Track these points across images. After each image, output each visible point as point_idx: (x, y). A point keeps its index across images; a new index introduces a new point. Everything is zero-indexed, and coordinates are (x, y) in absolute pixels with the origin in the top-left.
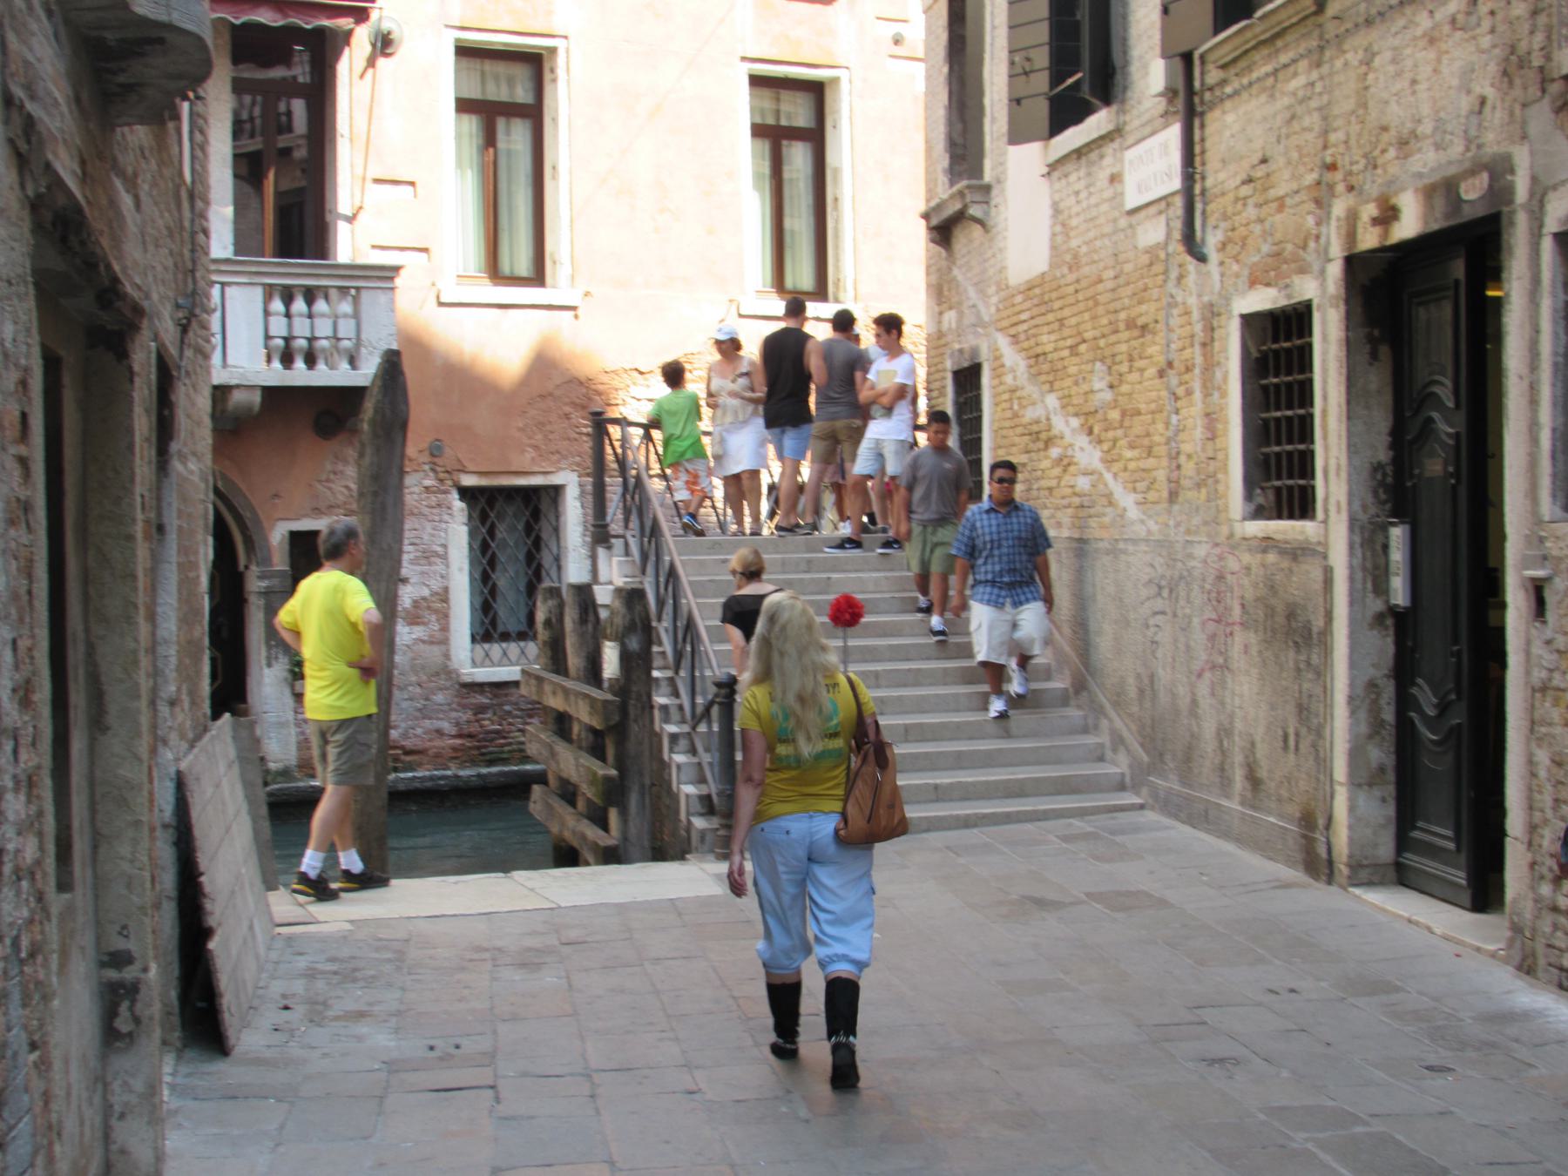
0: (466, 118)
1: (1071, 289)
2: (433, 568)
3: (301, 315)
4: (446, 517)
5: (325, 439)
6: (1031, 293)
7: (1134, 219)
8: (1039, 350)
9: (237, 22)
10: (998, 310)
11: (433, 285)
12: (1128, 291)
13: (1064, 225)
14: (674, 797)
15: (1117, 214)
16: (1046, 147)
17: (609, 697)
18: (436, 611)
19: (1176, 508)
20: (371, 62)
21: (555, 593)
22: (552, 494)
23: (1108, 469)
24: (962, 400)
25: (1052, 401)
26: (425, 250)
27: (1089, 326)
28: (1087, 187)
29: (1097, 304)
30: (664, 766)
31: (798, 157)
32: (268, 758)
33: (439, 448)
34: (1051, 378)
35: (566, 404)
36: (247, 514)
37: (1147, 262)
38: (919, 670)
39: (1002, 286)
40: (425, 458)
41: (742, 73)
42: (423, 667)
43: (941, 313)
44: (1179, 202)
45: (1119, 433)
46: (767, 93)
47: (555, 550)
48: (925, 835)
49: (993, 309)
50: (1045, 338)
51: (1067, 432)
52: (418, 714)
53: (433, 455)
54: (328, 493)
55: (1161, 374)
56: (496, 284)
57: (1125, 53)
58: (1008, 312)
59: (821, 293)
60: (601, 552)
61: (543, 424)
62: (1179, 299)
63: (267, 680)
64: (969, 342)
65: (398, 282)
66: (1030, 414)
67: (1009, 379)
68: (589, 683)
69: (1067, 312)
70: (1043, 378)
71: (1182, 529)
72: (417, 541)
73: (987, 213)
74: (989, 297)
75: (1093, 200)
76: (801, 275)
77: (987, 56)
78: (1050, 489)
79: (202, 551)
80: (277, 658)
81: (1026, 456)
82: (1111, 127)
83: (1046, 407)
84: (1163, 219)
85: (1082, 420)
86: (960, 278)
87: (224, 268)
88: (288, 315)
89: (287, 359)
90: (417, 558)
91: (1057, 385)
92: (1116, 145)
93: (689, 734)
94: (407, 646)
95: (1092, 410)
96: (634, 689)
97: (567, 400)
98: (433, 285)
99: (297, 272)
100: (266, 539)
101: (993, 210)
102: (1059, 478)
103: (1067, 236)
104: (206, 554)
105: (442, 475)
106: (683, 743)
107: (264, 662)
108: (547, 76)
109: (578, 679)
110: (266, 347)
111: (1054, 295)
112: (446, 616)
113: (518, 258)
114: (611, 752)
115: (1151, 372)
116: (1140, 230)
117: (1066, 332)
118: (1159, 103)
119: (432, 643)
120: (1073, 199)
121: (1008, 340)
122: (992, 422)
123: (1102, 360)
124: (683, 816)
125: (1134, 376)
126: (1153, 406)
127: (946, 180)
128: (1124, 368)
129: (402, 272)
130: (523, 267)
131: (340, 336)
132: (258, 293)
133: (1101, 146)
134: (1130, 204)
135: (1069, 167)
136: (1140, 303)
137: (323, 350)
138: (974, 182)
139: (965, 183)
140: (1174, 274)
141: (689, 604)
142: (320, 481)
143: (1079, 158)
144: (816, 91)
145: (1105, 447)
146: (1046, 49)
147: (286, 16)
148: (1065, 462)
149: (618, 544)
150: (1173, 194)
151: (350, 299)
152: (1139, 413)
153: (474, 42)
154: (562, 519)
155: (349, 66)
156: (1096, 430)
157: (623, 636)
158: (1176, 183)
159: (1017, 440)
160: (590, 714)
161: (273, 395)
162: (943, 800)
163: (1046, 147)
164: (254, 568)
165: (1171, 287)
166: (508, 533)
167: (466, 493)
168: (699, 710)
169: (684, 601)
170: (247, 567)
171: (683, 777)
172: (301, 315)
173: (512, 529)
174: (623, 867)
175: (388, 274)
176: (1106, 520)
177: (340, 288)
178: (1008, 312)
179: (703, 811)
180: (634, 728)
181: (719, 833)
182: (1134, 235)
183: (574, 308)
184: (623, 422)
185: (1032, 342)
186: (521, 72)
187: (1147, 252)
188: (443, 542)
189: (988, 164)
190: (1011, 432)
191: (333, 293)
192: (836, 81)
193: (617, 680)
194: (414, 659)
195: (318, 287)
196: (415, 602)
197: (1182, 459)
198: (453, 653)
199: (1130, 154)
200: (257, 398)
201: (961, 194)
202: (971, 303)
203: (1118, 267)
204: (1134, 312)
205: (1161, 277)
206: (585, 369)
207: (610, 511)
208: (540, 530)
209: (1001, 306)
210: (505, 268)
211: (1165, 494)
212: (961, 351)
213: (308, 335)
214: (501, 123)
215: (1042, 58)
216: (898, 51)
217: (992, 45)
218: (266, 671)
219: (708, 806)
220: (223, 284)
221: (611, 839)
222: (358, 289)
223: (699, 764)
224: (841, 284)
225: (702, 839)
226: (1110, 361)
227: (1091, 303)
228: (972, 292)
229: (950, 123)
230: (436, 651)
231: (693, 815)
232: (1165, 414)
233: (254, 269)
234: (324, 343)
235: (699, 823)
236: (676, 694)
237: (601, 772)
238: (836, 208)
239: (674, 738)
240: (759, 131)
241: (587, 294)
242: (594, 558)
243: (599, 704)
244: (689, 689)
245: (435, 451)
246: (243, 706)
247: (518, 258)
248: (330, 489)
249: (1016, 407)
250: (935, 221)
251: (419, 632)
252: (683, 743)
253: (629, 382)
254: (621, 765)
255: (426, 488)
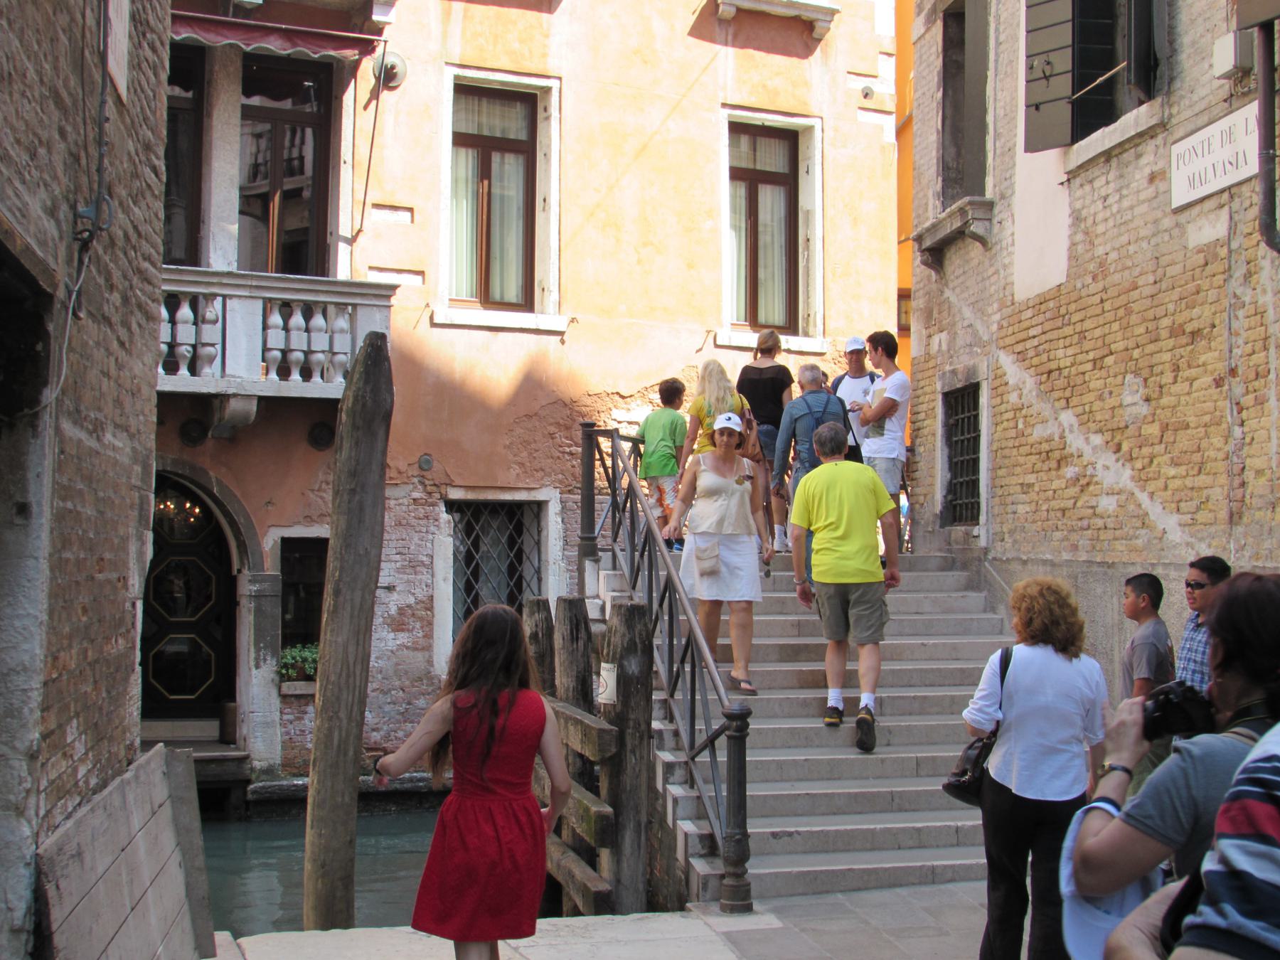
0: (462, 151)
1: (1097, 299)
2: (419, 577)
3: (299, 329)
4: (432, 529)
5: (320, 450)
6: (1043, 307)
7: (1182, 218)
8: (1053, 365)
9: (249, 49)
10: (1001, 328)
11: (428, 305)
12: (1175, 295)
13: (1087, 233)
14: (672, 834)
15: (1159, 214)
16: (1066, 154)
17: (606, 726)
18: (421, 619)
19: (1239, 530)
20: (375, 95)
21: (543, 605)
22: (535, 508)
23: (1143, 489)
24: (952, 421)
25: (1067, 417)
26: (421, 273)
27: (1119, 336)
28: (1119, 190)
29: (1129, 312)
30: (655, 796)
31: (771, 200)
32: (252, 756)
33: (428, 462)
34: (1068, 393)
35: (551, 424)
36: (241, 520)
37: (1202, 262)
38: (925, 697)
39: (1007, 302)
40: (415, 471)
41: (724, 116)
42: (406, 673)
43: (930, 336)
44: (1258, 186)
45: (1159, 449)
46: (745, 140)
47: (536, 564)
48: (950, 886)
49: (994, 327)
50: (1060, 353)
51: (1087, 450)
52: (400, 717)
53: (421, 468)
54: (320, 501)
55: (1218, 383)
56: (486, 308)
57: (1172, 42)
58: (1016, 328)
59: (791, 326)
60: (588, 565)
61: (529, 444)
62: (1247, 299)
63: (254, 681)
64: (963, 362)
65: (393, 300)
66: (1038, 433)
67: (1013, 398)
68: (578, 705)
69: (1088, 324)
70: (1056, 394)
71: (1247, 554)
72: (406, 551)
73: (989, 230)
74: (989, 316)
75: (1126, 203)
76: (772, 309)
77: (990, 74)
78: (1064, 511)
79: (133, 548)
80: (265, 660)
81: (1034, 476)
82: (1153, 121)
83: (1060, 424)
84: (1224, 213)
85: (1108, 436)
86: (953, 299)
87: (225, 281)
88: (286, 328)
89: (284, 372)
90: (404, 567)
91: (1074, 401)
92: (1159, 140)
93: (686, 763)
94: (392, 651)
95: (1122, 425)
96: (632, 716)
97: (552, 421)
98: (428, 305)
99: (297, 287)
100: (259, 544)
101: (996, 228)
102: (1076, 499)
103: (1092, 243)
104: (141, 554)
105: (429, 488)
106: (679, 773)
107: (252, 663)
108: (541, 115)
109: (566, 700)
110: (264, 360)
111: (1073, 307)
112: (430, 624)
113: (509, 284)
114: (604, 785)
115: (1207, 380)
116: (1191, 228)
117: (1087, 345)
118: (1221, 86)
119: (416, 649)
120: (1100, 205)
121: (1012, 357)
122: (991, 443)
123: (1136, 373)
124: (680, 854)
125: (1181, 387)
126: (1207, 418)
127: (938, 204)
128: (1168, 378)
129: (398, 291)
130: (513, 292)
131: (336, 350)
132: (259, 305)
133: (1137, 145)
134: (1178, 200)
135: (1095, 171)
136: (1190, 307)
137: (319, 363)
138: (977, 198)
139: (967, 199)
140: (1239, 272)
141: (689, 620)
142: (313, 490)
143: (1108, 161)
144: (791, 139)
145: (1139, 465)
146: (1069, 51)
147: (295, 45)
148: (1083, 481)
149: (606, 557)
150: (1249, 180)
151: (347, 316)
152: (1187, 427)
153: (473, 79)
154: (544, 534)
155: (353, 98)
156: (1125, 447)
157: (622, 657)
158: (1252, 166)
159: (1021, 460)
160: (582, 742)
161: (269, 405)
162: (965, 845)
163: (1066, 154)
164: (246, 571)
165: (1235, 285)
166: (493, 547)
167: (452, 506)
168: (700, 739)
169: (682, 617)
170: (239, 571)
171: (680, 812)
172: (299, 329)
173: (496, 542)
174: (618, 918)
175: (386, 292)
176: (1139, 542)
177: (337, 304)
178: (1016, 328)
179: (703, 852)
180: (631, 760)
181: (727, 881)
182: (1183, 233)
183: (561, 333)
184: (612, 434)
185: (1044, 357)
186: (518, 111)
187: (1199, 251)
188: (430, 552)
189: (989, 182)
190: (1015, 452)
191: (331, 310)
192: (810, 129)
193: (614, 706)
194: (397, 664)
195: (317, 303)
196: (400, 609)
197: (1249, 475)
198: (435, 659)
199: (1177, 149)
200: (253, 407)
201: (962, 211)
202: (966, 324)
203: (1160, 271)
204: (1180, 319)
205: (1222, 277)
206: (571, 391)
207: (598, 524)
208: (522, 543)
209: (1005, 323)
210: (496, 294)
211: (1223, 515)
212: (954, 372)
213: (305, 349)
214: (496, 157)
215: (1064, 61)
216: (867, 103)
217: (996, 61)
218: (254, 671)
219: (709, 846)
220: (225, 297)
221: (601, 882)
222: (355, 306)
223: (699, 798)
224: (811, 319)
225: (705, 886)
226: (1146, 374)
227: (1121, 312)
228: (967, 312)
229: (943, 146)
230: (420, 656)
231: (693, 856)
232: (1224, 426)
233: (254, 283)
234: (320, 356)
235: (700, 866)
236: (670, 717)
237: (594, 809)
238: (807, 248)
239: (669, 767)
240: (737, 174)
241: (573, 320)
242: (581, 571)
243: (594, 733)
244: (688, 716)
245: (424, 465)
246: (233, 704)
247: (509, 284)
248: (322, 498)
249: (1020, 426)
250: (928, 243)
251: (403, 638)
252: (679, 773)
253: (611, 405)
254: (615, 801)
255: (414, 500)
